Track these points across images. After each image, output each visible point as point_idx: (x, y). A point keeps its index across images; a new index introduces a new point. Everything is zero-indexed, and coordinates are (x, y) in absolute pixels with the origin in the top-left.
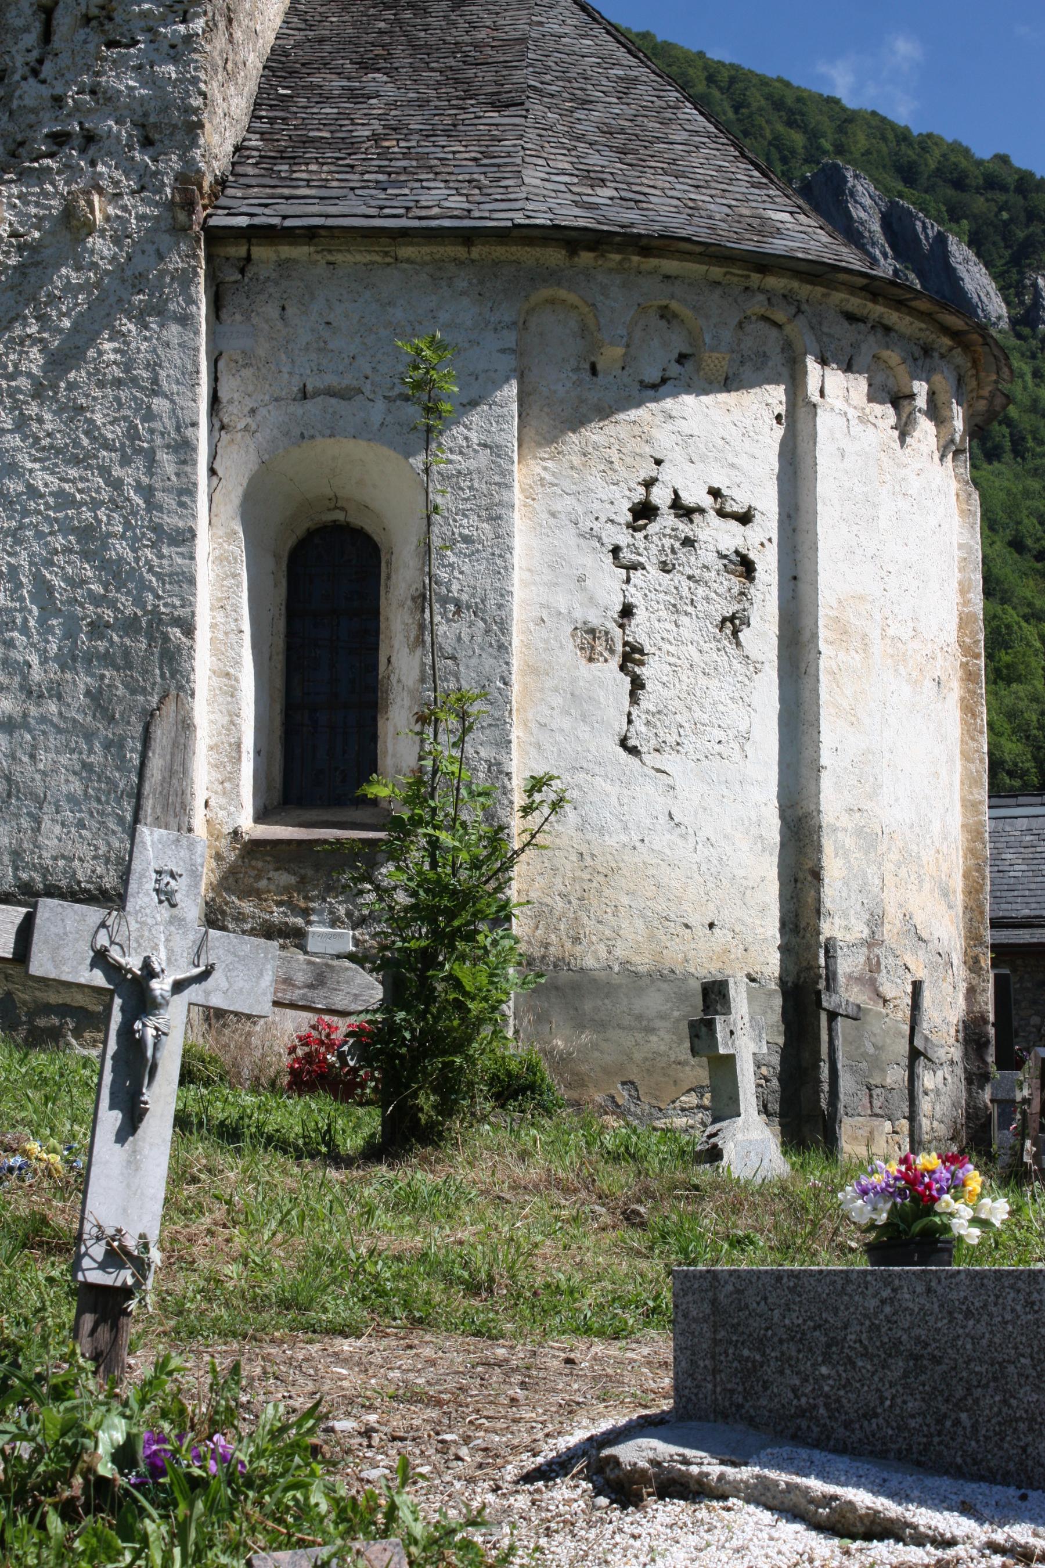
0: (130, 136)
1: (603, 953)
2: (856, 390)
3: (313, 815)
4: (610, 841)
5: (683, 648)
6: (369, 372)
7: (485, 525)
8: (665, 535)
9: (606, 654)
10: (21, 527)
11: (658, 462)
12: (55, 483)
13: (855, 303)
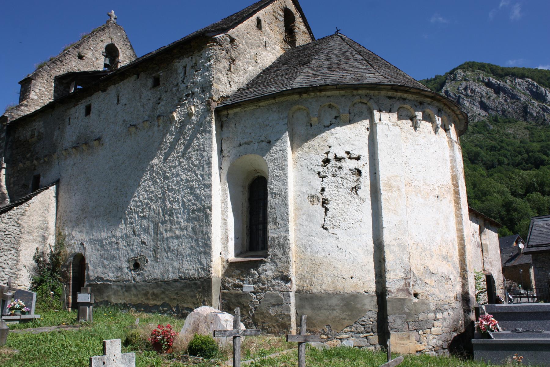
1: (319, 288)
10: (180, 189)
11: (330, 147)
13: (390, 94)
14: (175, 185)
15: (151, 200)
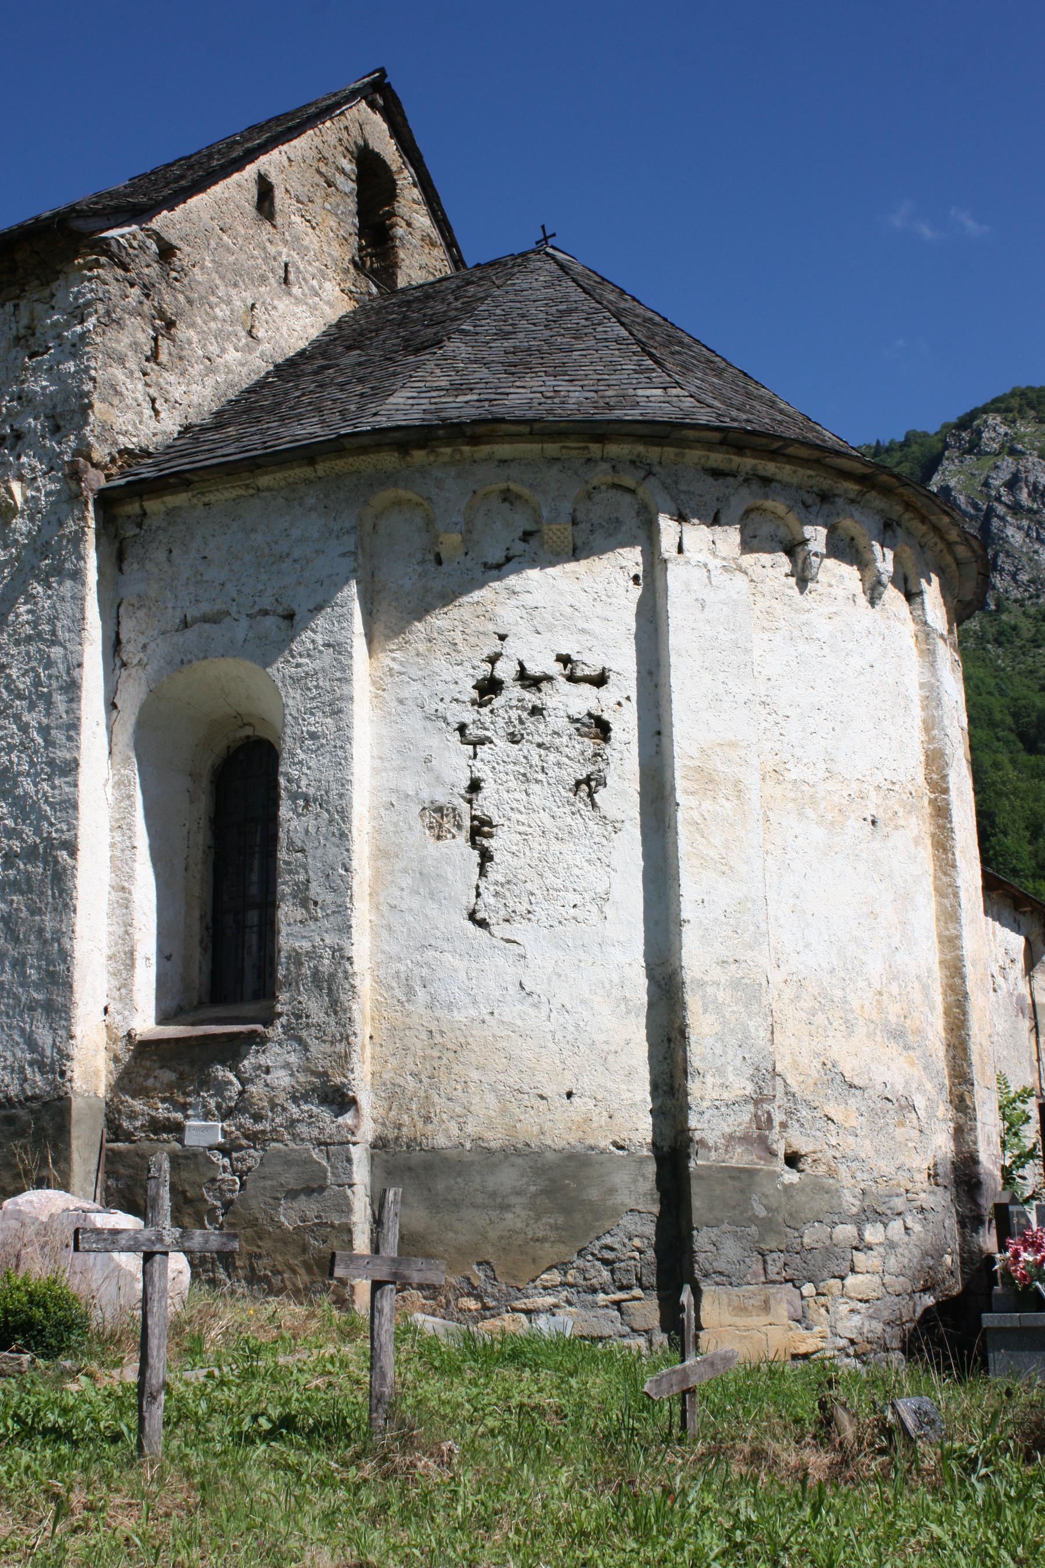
0: (43, 427)
1: (454, 1130)
2: (725, 541)
4: (458, 1016)
5: (535, 816)
6: (234, 595)
7: (329, 720)
8: (511, 707)
9: (454, 830)
11: (502, 638)
13: (717, 459)
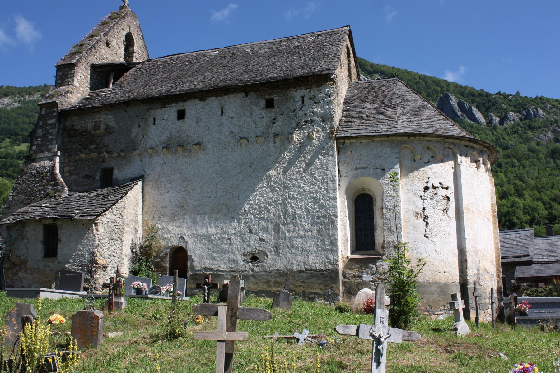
3: (362, 252)
12: (308, 189)
13: (467, 143)
14: (296, 195)
15: (270, 205)
